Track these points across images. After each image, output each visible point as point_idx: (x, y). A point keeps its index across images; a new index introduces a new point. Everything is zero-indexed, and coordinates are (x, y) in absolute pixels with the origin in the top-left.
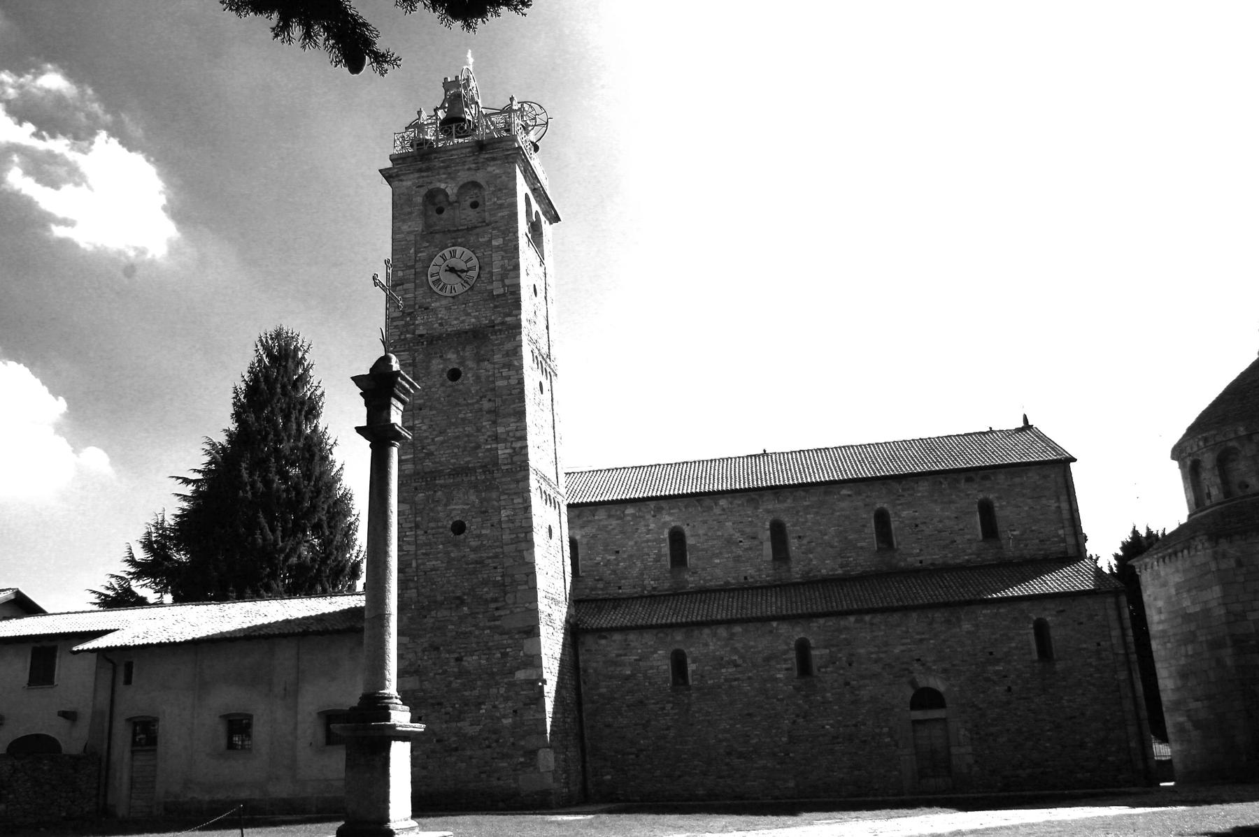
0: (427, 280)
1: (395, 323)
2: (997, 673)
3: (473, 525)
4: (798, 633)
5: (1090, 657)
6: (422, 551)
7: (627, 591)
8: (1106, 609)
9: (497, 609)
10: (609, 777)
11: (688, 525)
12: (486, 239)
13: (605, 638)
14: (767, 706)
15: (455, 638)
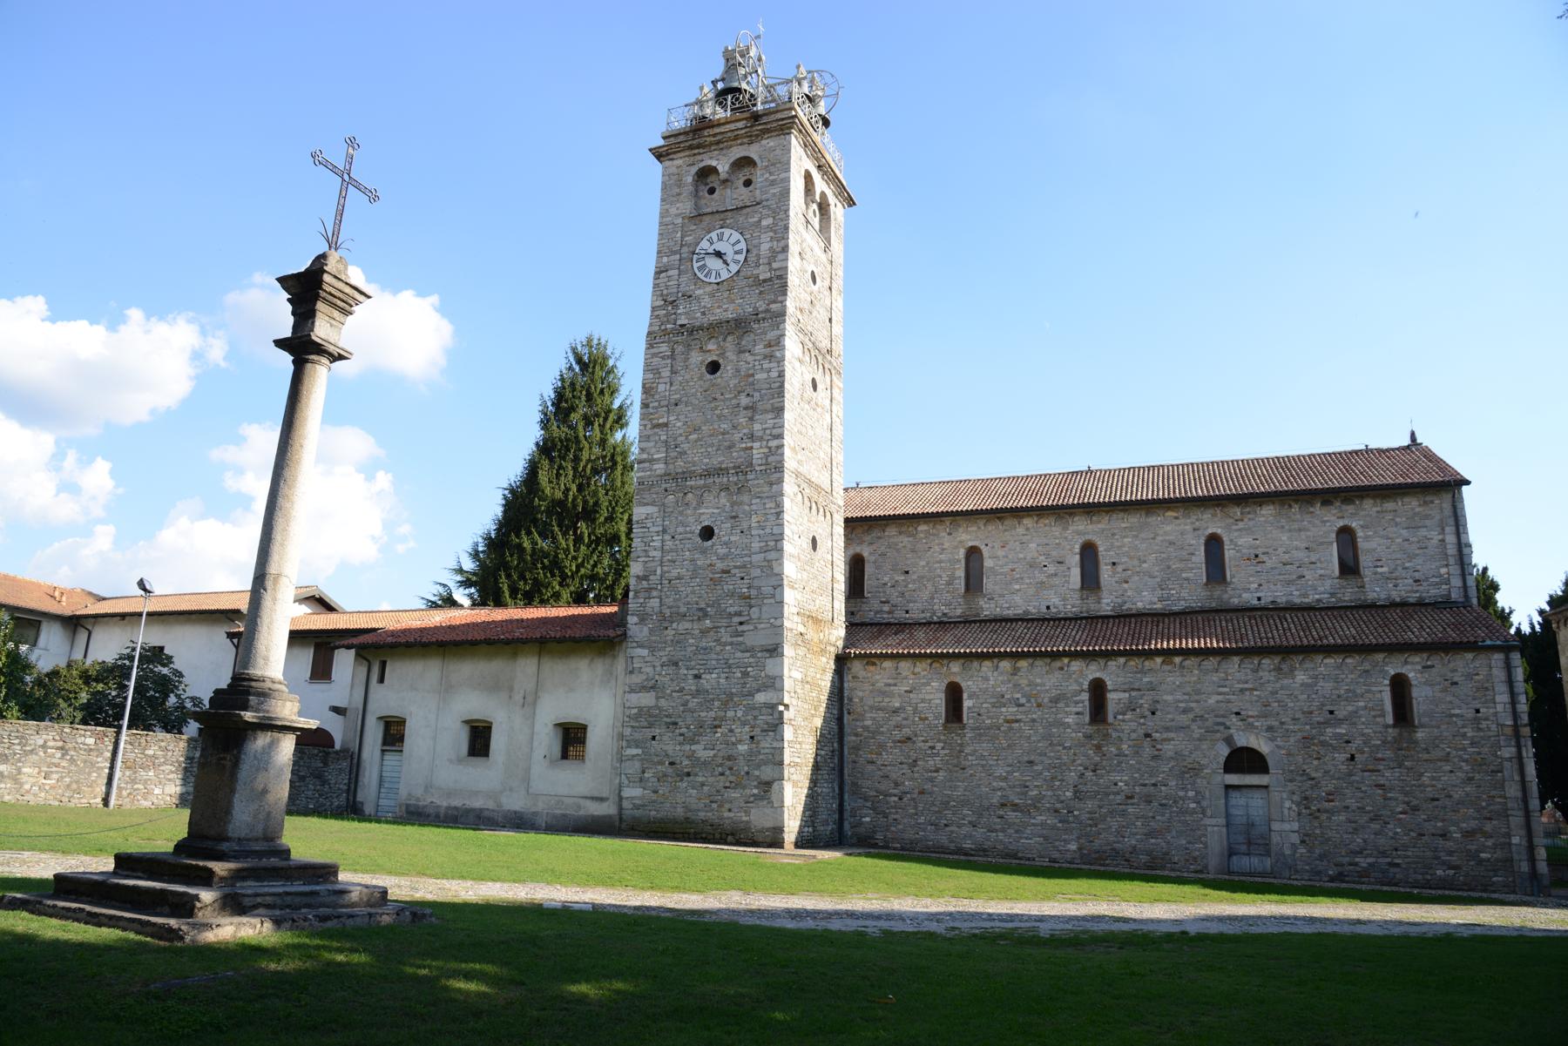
1: (657, 313)
2: (1337, 736)
3: (722, 531)
4: (1093, 671)
5: (1463, 727)
7: (916, 615)
8: (1491, 667)
9: (741, 623)
10: (868, 819)
13: (874, 664)
14: (1052, 754)
15: (695, 654)
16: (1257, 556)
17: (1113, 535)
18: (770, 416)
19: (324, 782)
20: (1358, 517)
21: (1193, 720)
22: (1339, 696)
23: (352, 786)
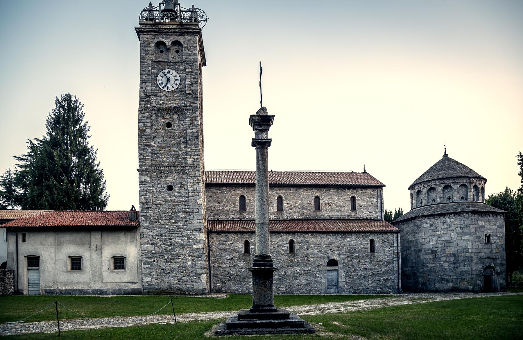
0: (157, 82)
1: (142, 99)
2: (356, 256)
3: (177, 188)
4: (290, 237)
6: (155, 196)
7: (223, 218)
9: (186, 221)
10: (219, 284)
11: (247, 195)
12: (183, 68)
15: (169, 232)
16: (329, 203)
17: (287, 194)
18: (194, 146)
19: (5, 283)
20: (357, 194)
21: (319, 252)
22: (357, 245)
23: (16, 284)
